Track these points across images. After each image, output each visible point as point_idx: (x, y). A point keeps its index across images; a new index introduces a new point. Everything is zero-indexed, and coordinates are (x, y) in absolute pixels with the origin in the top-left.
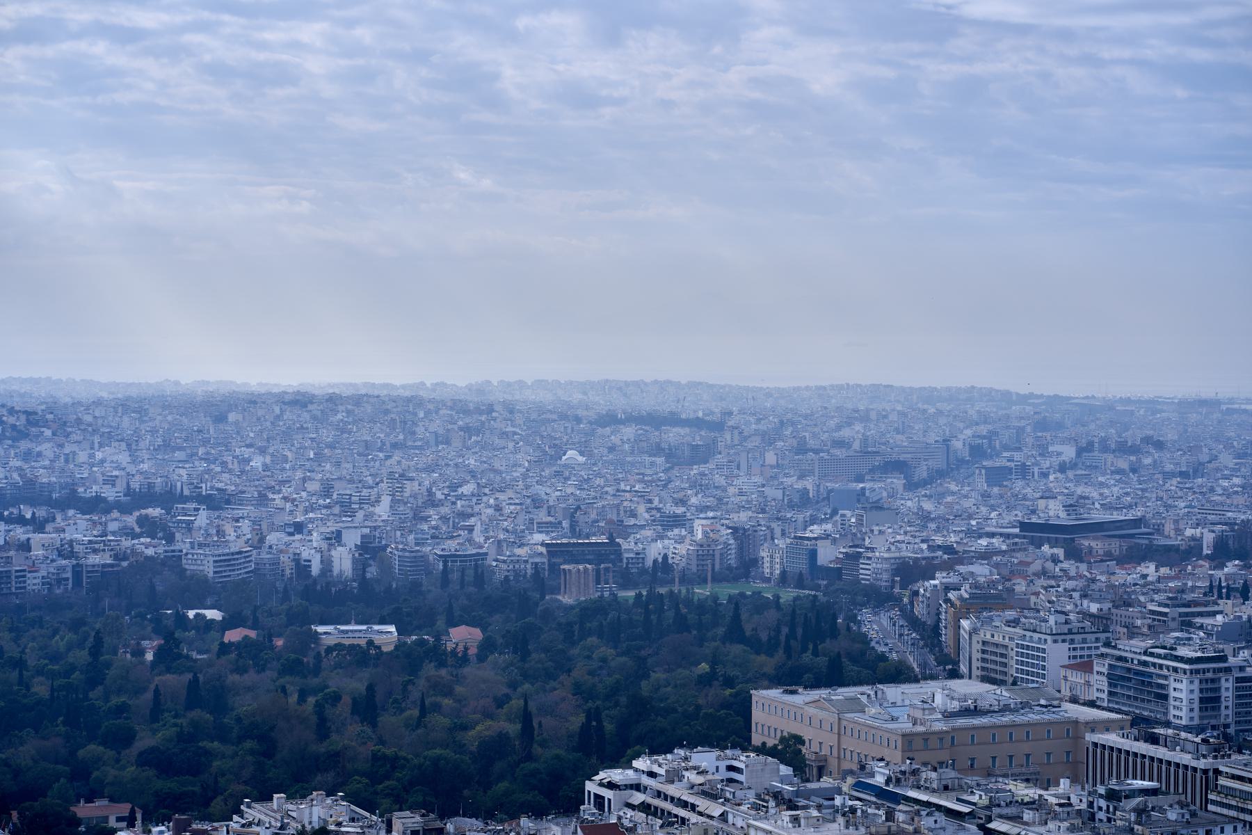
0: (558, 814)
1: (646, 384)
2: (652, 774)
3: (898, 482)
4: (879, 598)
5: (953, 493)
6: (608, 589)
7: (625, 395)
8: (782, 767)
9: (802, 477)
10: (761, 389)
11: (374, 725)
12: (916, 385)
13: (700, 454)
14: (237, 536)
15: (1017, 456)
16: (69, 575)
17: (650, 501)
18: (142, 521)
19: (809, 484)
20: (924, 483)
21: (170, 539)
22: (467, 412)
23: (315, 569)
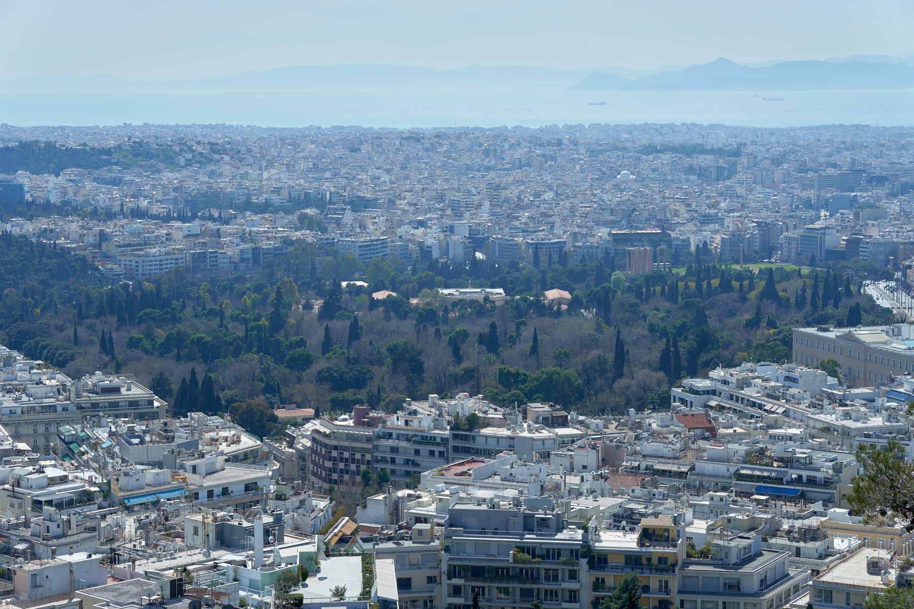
1: (677, 126)
2: (725, 382)
6: (663, 265)
7: (661, 134)
8: (829, 378)
10: (766, 129)
11: (498, 354)
12: (888, 125)
13: (721, 174)
14: (375, 226)
16: (250, 256)
17: (689, 205)
21: (324, 230)
22: (541, 145)
23: (435, 254)
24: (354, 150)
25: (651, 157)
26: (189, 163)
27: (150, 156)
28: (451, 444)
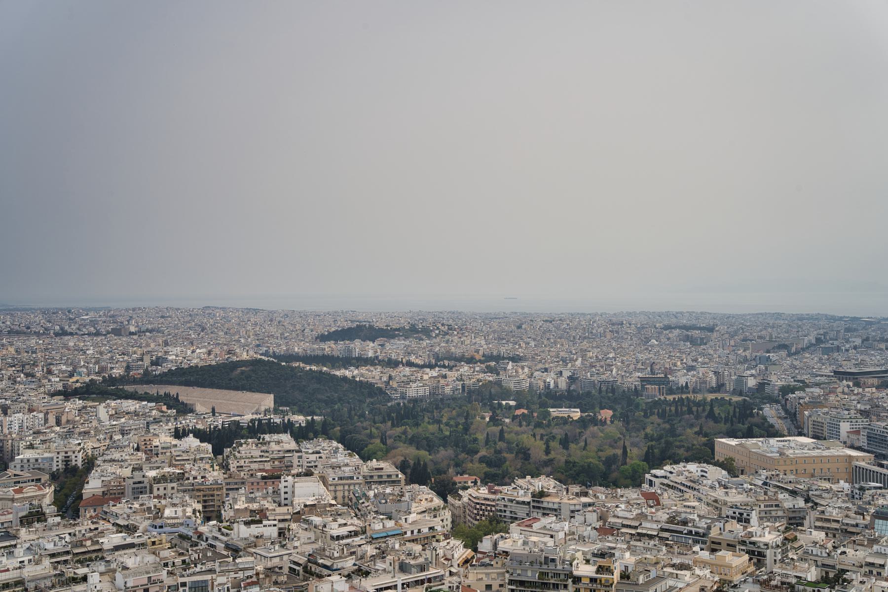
0: (633, 487)
3: (783, 353)
4: (772, 400)
5: (807, 358)
9: (744, 351)
13: (703, 342)
15: (836, 343)
18: (487, 367)
19: (748, 353)
20: (796, 353)
21: (498, 374)
22: (613, 324)
23: (552, 386)
25: (667, 332)
26: (437, 335)
27: (417, 332)
28: (532, 504)
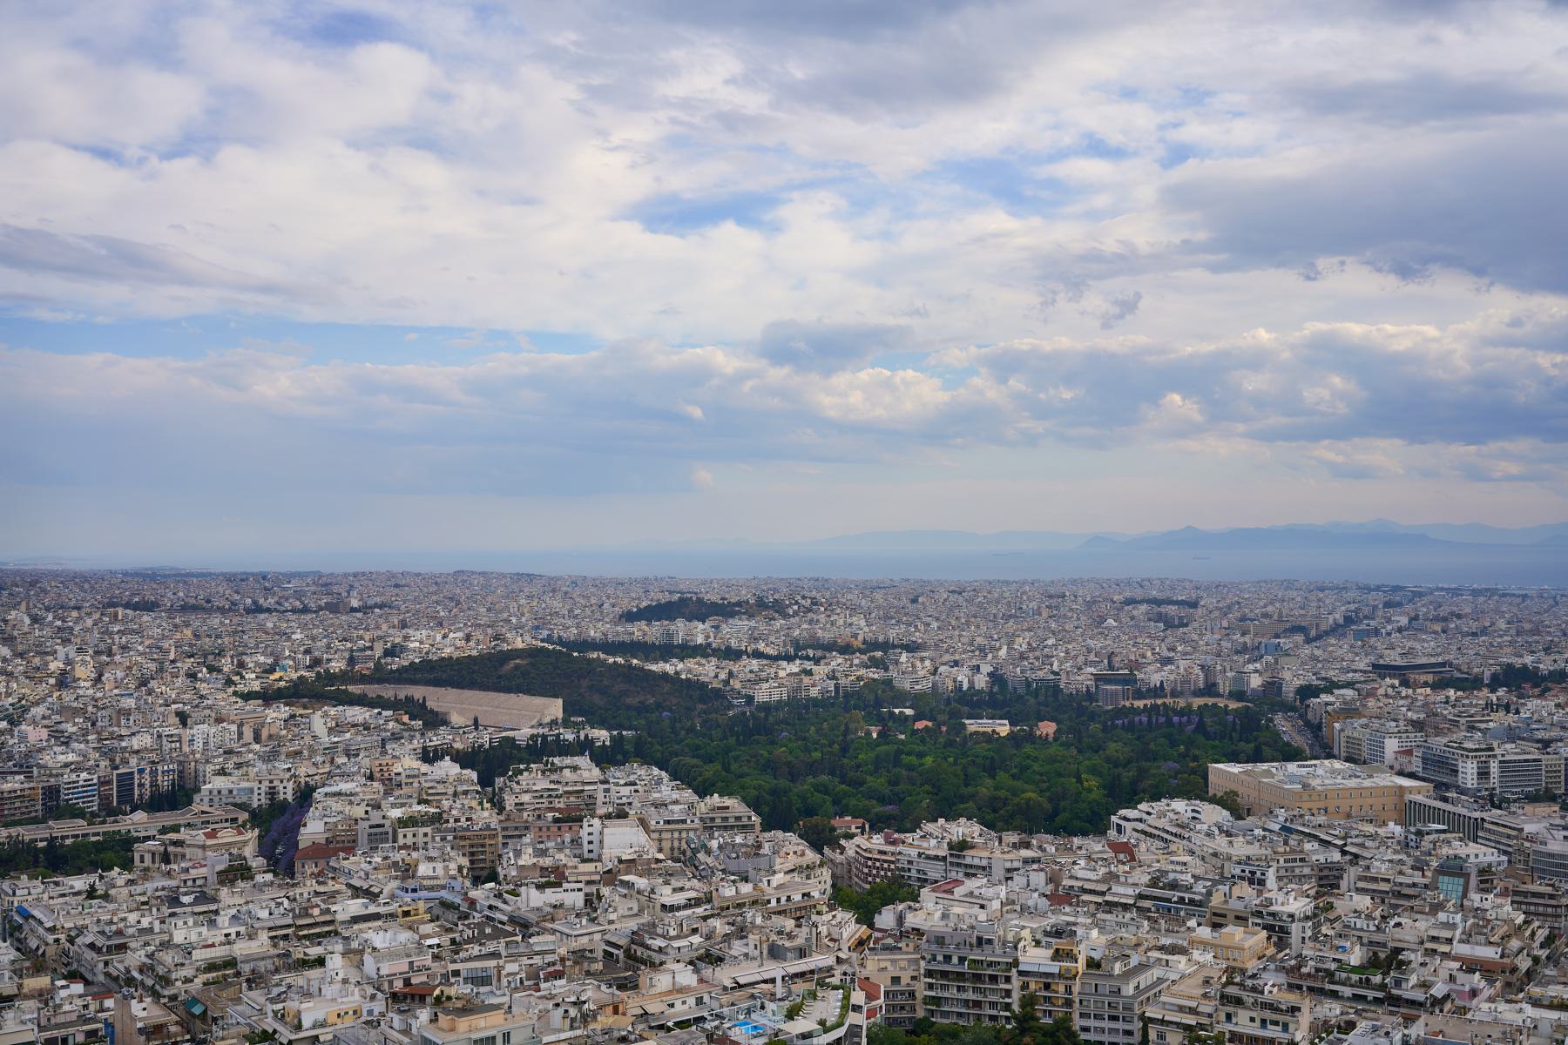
2: (1149, 813)
24: (914, 601)
26: (796, 613)
